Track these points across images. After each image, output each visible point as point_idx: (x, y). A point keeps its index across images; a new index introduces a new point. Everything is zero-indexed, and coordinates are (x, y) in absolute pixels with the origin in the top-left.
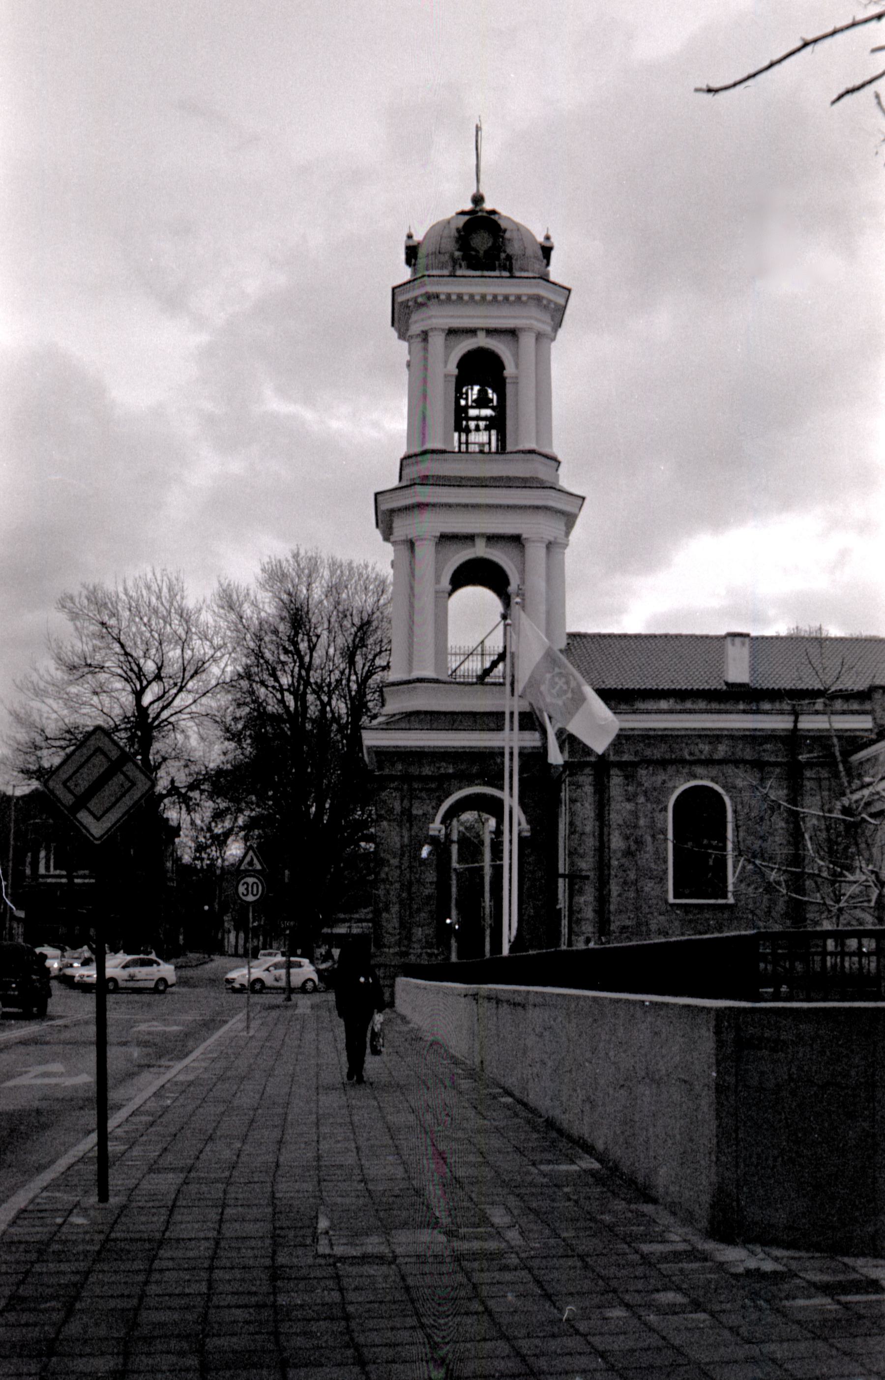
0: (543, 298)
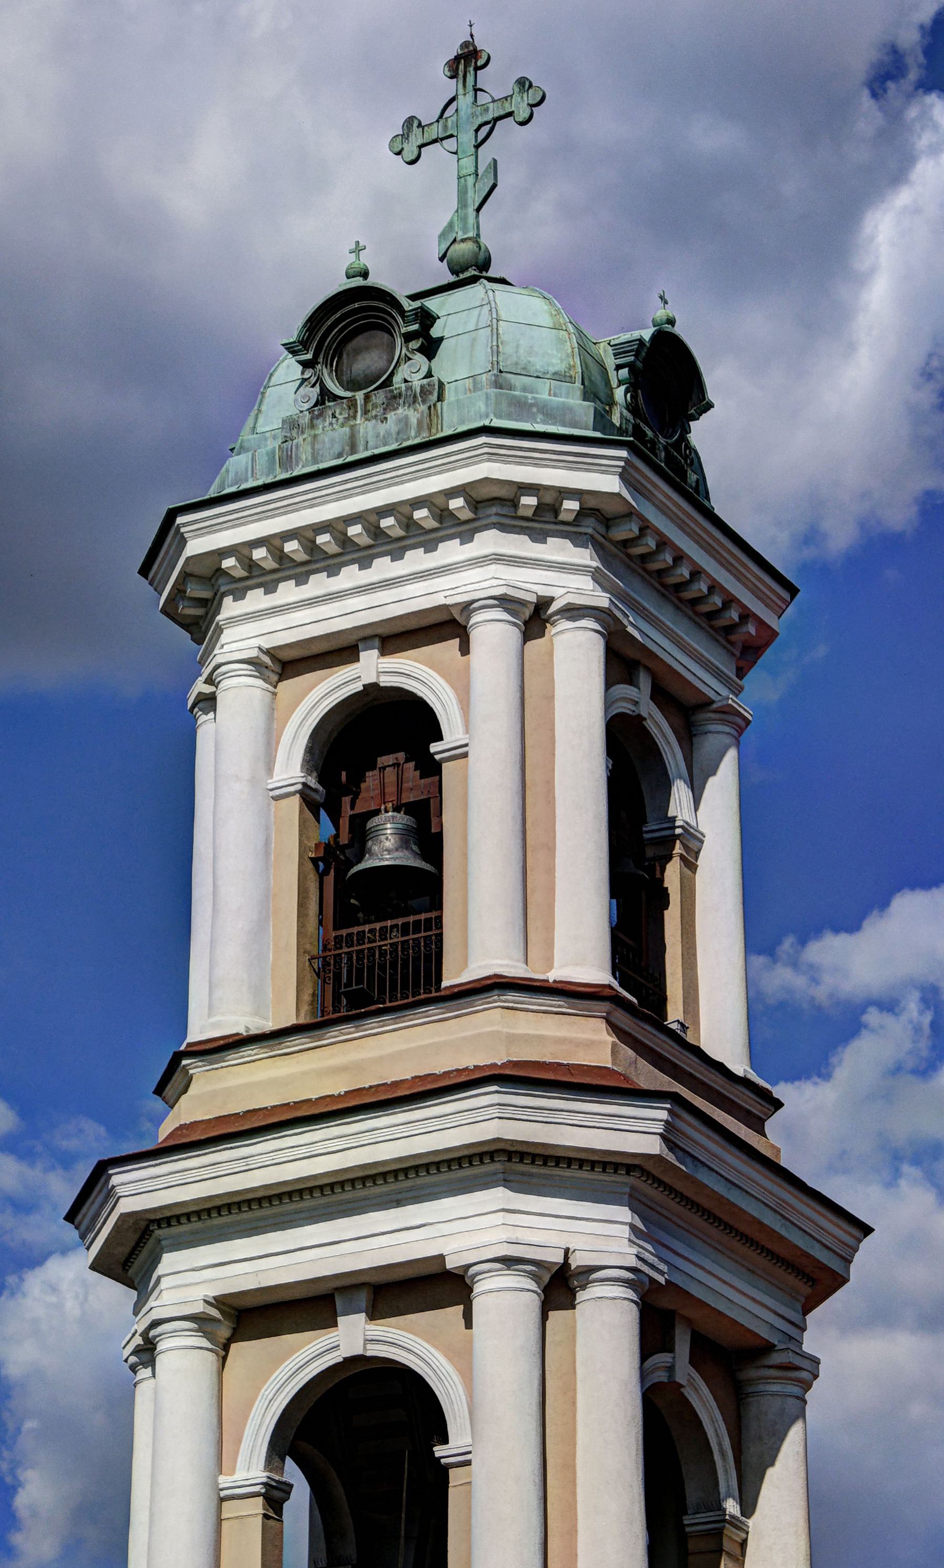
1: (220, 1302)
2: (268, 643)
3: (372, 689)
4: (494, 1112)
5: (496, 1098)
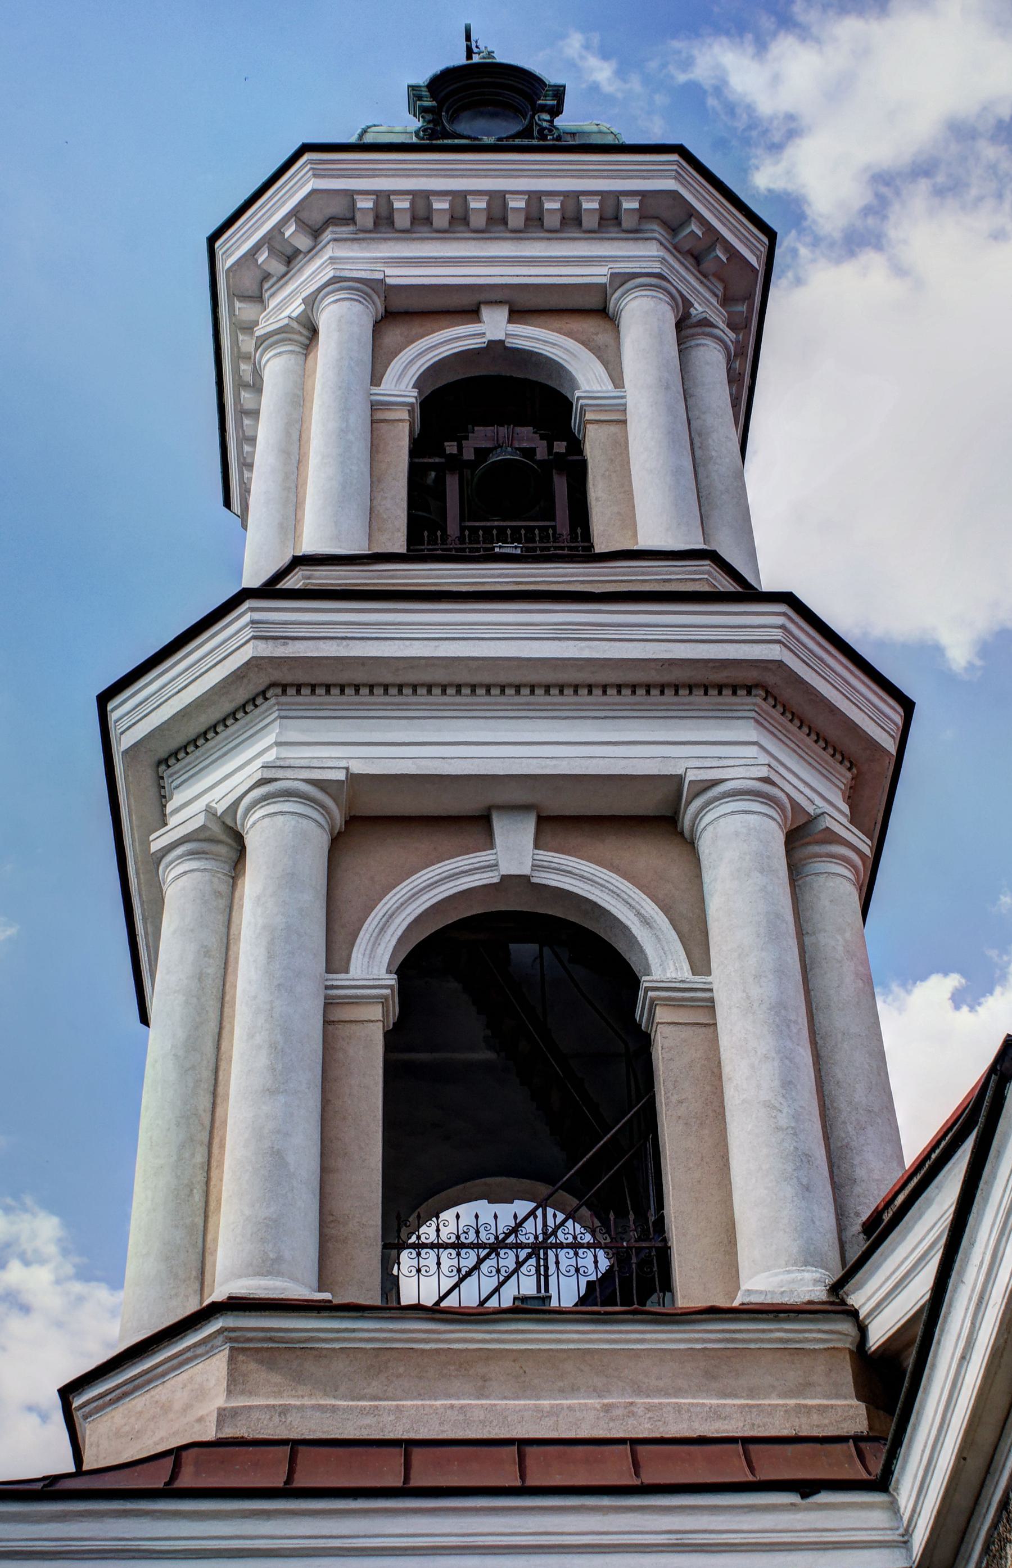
0: (692, 213)
1: (354, 779)
2: (358, 768)
3: (496, 347)
4: (778, 634)
5: (780, 620)
